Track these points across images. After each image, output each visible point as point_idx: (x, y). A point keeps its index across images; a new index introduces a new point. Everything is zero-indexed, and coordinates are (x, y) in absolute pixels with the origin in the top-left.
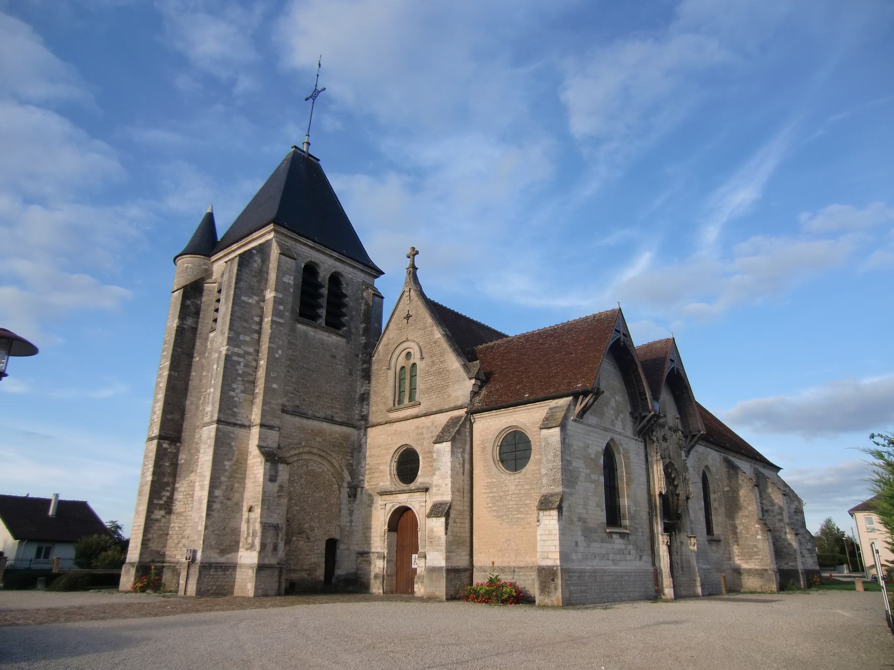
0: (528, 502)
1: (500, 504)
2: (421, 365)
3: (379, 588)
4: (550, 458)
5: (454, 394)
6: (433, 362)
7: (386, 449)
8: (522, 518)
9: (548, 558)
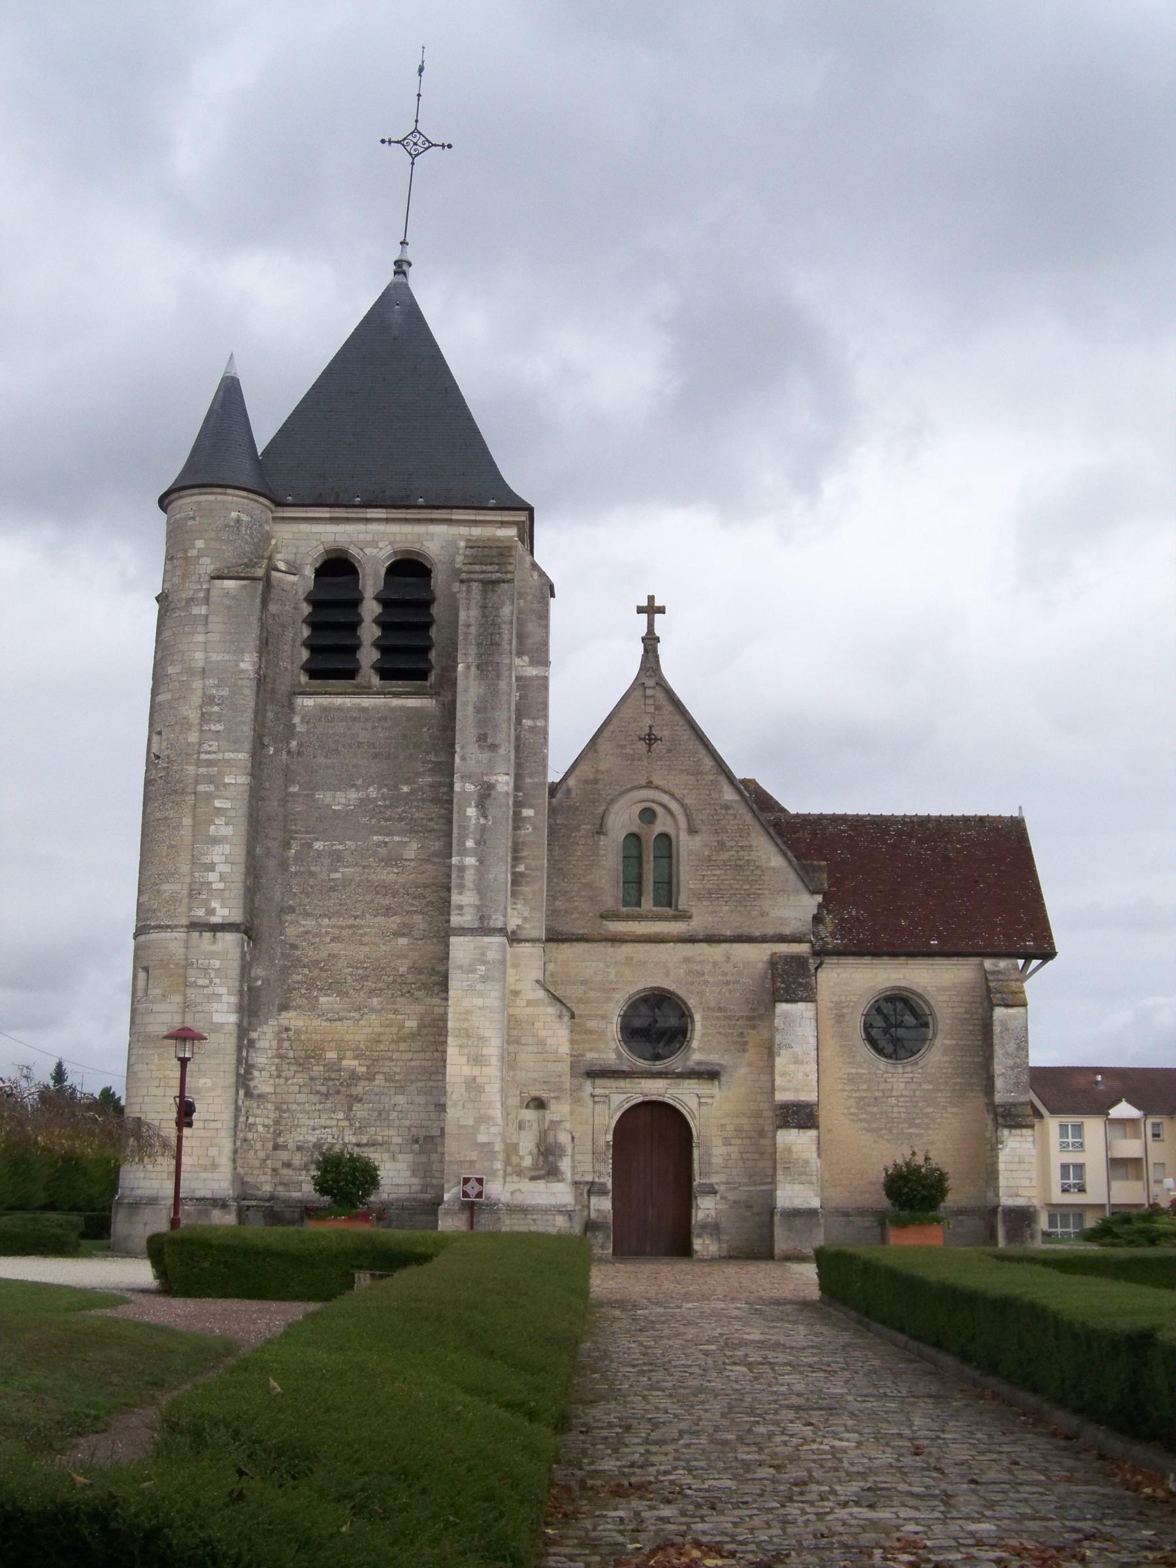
0: (930, 1110)
1: (875, 1110)
2: (687, 845)
3: (603, 1247)
4: (1010, 1050)
5: (774, 913)
6: (721, 844)
7: (604, 991)
8: (917, 1135)
9: (1018, 1195)
